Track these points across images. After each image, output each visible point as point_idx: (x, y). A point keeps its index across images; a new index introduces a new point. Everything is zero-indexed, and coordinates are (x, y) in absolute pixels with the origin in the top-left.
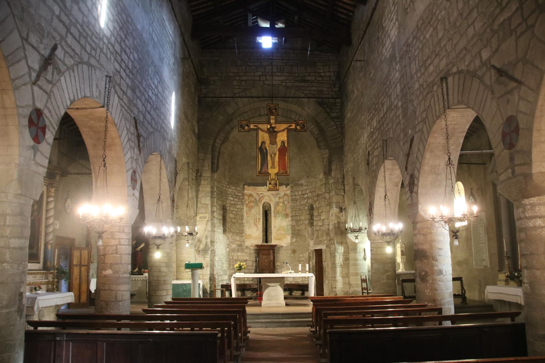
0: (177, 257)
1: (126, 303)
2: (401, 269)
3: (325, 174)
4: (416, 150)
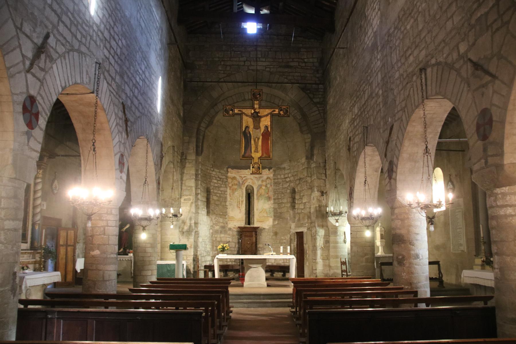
0: (161, 239)
1: (113, 283)
2: (380, 252)
3: (307, 158)
4: (396, 138)
